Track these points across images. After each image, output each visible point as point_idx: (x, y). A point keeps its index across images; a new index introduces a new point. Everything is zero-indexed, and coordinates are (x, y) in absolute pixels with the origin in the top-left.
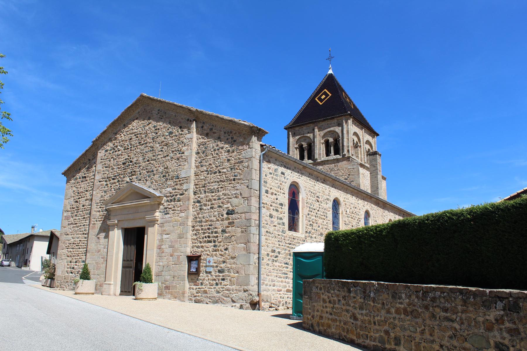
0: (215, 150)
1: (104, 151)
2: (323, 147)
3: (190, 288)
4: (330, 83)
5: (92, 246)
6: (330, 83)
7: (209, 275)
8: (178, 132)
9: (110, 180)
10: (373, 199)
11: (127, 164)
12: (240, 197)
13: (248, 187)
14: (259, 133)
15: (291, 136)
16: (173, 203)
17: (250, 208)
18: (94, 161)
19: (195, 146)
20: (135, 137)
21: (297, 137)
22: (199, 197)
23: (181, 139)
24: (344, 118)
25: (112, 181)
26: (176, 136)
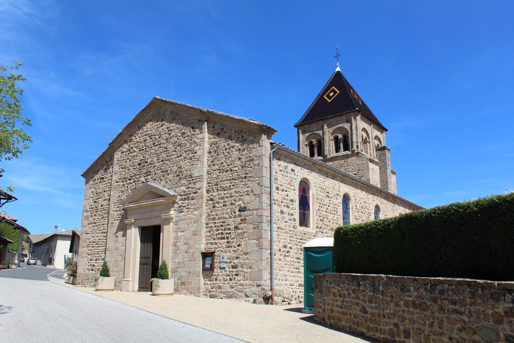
0: (226, 149)
1: (120, 153)
2: (333, 144)
3: (205, 284)
4: (338, 80)
5: (111, 244)
6: (338, 80)
7: (223, 271)
8: (190, 132)
9: (126, 181)
10: (383, 193)
11: (142, 164)
12: (251, 194)
13: (259, 184)
14: (269, 131)
15: (301, 133)
16: (187, 201)
17: (262, 204)
18: (111, 162)
21: (307, 135)
24: (352, 114)
25: (129, 181)
26: (189, 136)
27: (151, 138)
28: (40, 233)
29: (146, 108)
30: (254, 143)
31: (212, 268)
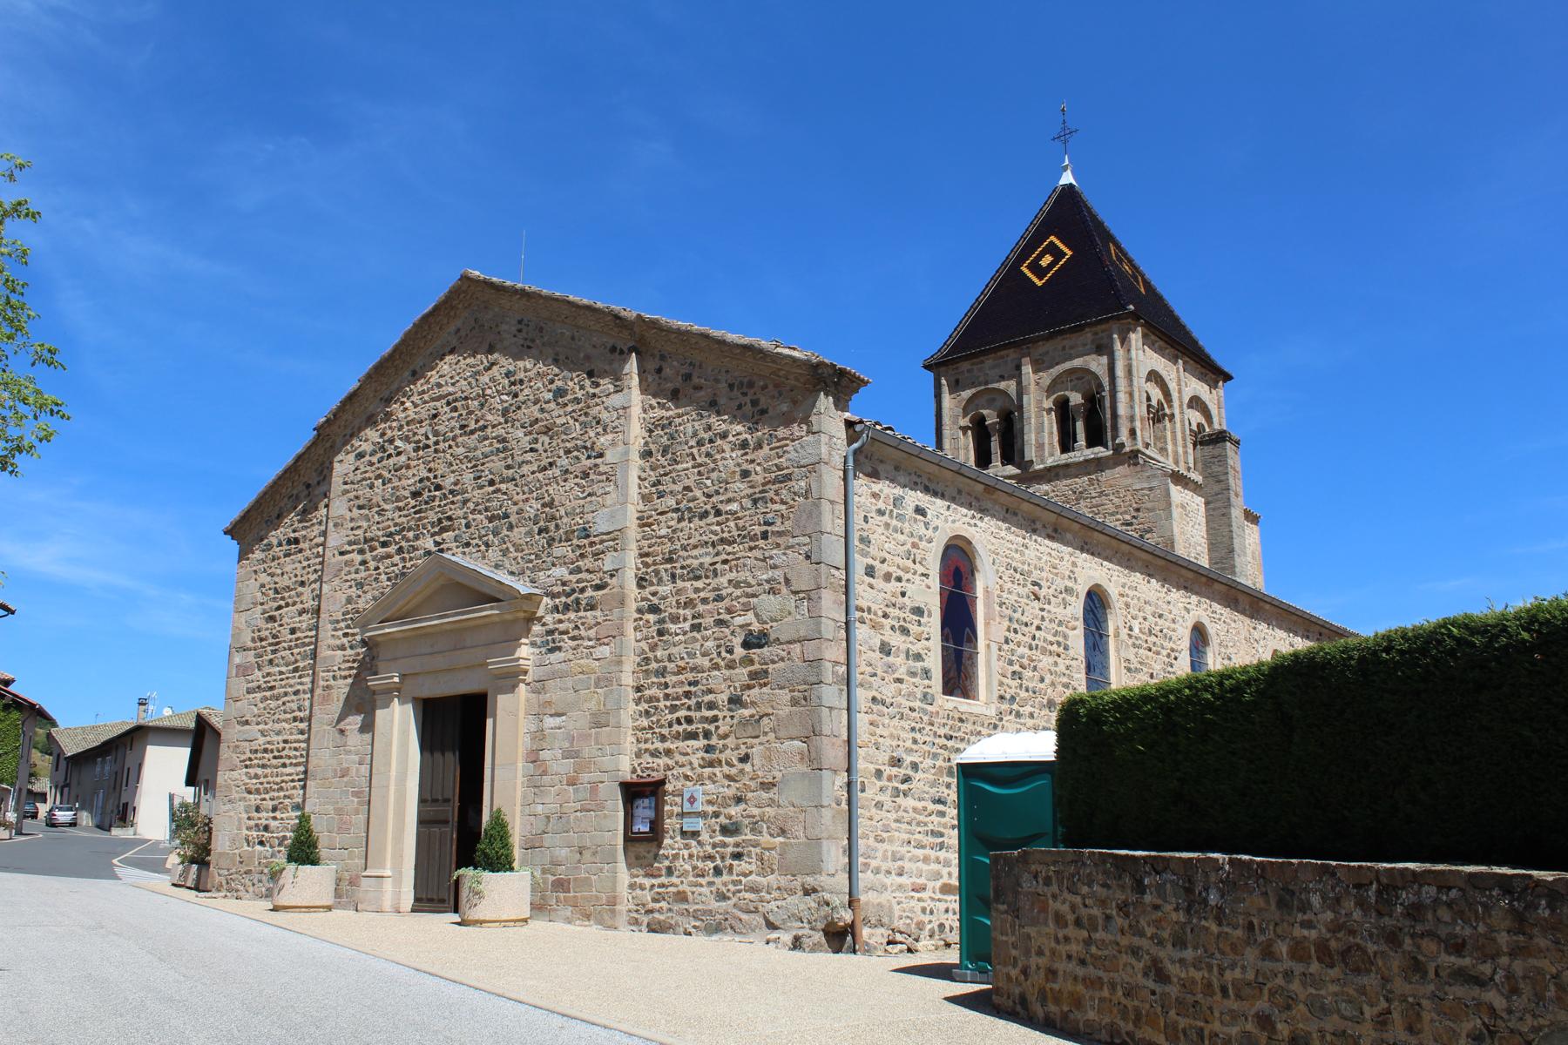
0: (700, 443)
1: (351, 457)
2: (1050, 423)
3: (632, 886)
6: (1068, 215)
7: (694, 843)
8: (582, 387)
9: (372, 549)
10: (1217, 586)
11: (426, 495)
12: (784, 590)
13: (808, 557)
14: (841, 384)
15: (945, 389)
16: (572, 615)
18: (323, 488)
19: (636, 432)
20: (446, 409)
21: (967, 394)
23: (594, 411)
24: (1115, 325)
25: (381, 551)
27: (455, 409)
28: (88, 721)
30: (794, 421)
31: (656, 833)
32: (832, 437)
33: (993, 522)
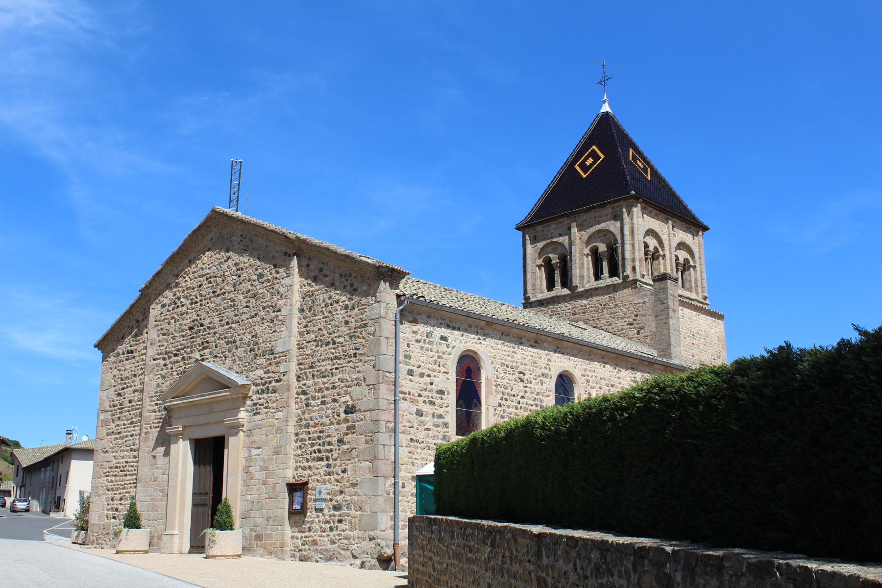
0: (326, 306)
1: (159, 306)
2: (588, 263)
3: (292, 537)
4: (606, 133)
5: (145, 471)
6: (606, 133)
8: (271, 274)
9: (170, 358)
10: (656, 366)
11: (196, 328)
12: (363, 384)
13: (374, 367)
14: (394, 276)
15: (528, 242)
16: (265, 395)
17: (378, 402)
18: (144, 323)
19: (296, 299)
20: (206, 282)
21: (540, 245)
22: (304, 385)
23: (276, 287)
24: (624, 203)
25: (174, 359)
26: (268, 281)
27: (210, 282)
28: (37, 445)
29: (200, 227)
31: (303, 511)
32: (387, 304)
33: (493, 341)
